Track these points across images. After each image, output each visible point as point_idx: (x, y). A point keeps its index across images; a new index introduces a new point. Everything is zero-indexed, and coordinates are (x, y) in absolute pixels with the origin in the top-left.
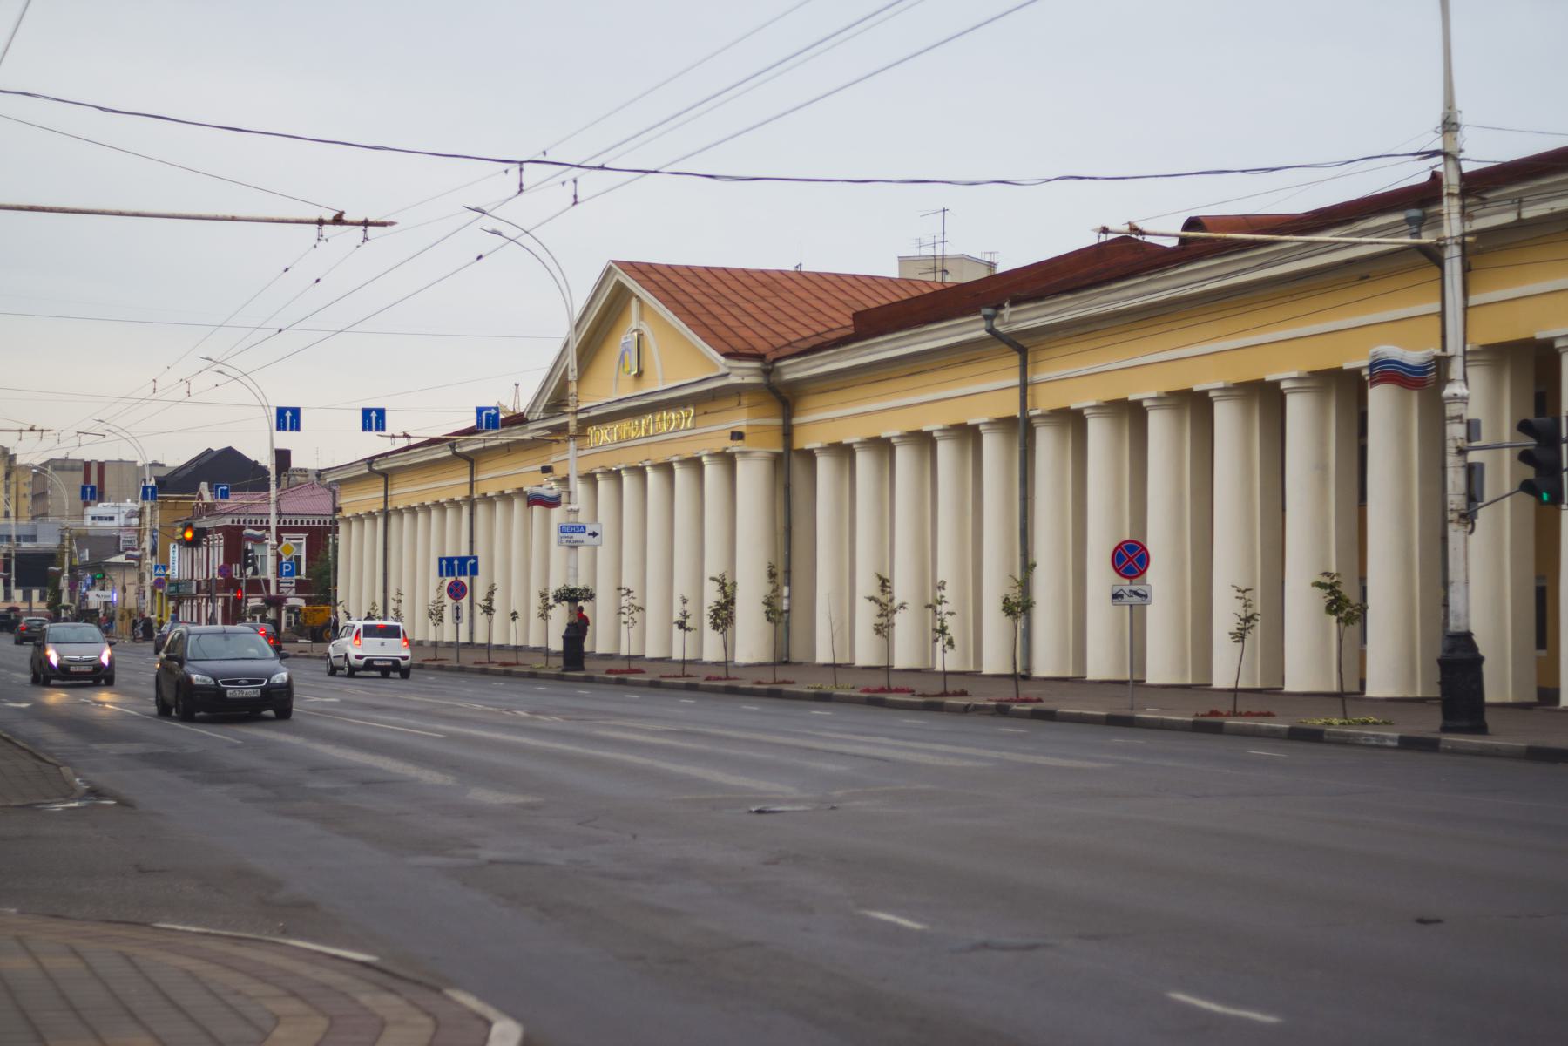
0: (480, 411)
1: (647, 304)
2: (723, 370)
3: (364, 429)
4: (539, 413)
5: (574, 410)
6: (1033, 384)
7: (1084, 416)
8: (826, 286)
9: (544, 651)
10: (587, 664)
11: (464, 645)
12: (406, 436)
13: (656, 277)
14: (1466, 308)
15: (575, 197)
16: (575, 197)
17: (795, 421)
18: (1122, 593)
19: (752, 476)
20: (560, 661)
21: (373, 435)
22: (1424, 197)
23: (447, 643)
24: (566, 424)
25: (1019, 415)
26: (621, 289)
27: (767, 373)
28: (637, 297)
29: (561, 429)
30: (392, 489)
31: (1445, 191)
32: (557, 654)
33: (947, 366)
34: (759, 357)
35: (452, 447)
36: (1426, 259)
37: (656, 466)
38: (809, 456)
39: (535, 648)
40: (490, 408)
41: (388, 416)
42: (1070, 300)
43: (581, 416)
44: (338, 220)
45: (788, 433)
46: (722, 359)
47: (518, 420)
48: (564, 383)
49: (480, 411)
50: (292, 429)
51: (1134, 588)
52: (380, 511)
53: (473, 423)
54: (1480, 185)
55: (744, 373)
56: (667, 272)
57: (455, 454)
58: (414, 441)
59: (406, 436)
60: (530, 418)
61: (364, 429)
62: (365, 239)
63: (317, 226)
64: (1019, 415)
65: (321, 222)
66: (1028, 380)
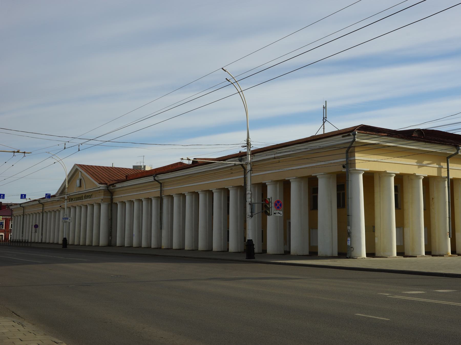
0: (46, 194)
1: (83, 174)
2: (98, 186)
3: (21, 198)
4: (58, 195)
5: (67, 194)
6: (163, 190)
7: (317, 178)
8: (120, 170)
9: (57, 244)
10: (68, 246)
11: (40, 243)
12: (29, 199)
13: (84, 167)
14: (251, 176)
15: (79, 149)
16: (79, 149)
17: (113, 197)
18: (276, 213)
19: (104, 207)
20: (62, 246)
21: (23, 200)
22: (241, 156)
23: (36, 242)
24: (65, 197)
25: (160, 196)
26: (77, 169)
27: (108, 187)
28: (81, 172)
29: (64, 198)
30: (25, 210)
31: (247, 154)
32: (61, 244)
33: (401, 157)
34: (106, 184)
35: (39, 201)
36: (241, 166)
37: (83, 205)
38: (26, 215)
39: (52, 243)
40: (48, 194)
41: (26, 196)
42: (171, 174)
43: (68, 195)
44: (18, 152)
45: (112, 199)
46: (98, 184)
47: (54, 196)
48: (64, 188)
49: (46, 194)
50: (2, 198)
51: (279, 212)
52: (41, 212)
53: (45, 196)
54: (254, 153)
55: (102, 187)
56: (87, 167)
57: (39, 203)
58: (31, 200)
59: (29, 199)
60: (56, 196)
61: (21, 198)
62: (25, 156)
63: (13, 153)
64: (160, 196)
65: (14, 152)
66: (162, 189)
